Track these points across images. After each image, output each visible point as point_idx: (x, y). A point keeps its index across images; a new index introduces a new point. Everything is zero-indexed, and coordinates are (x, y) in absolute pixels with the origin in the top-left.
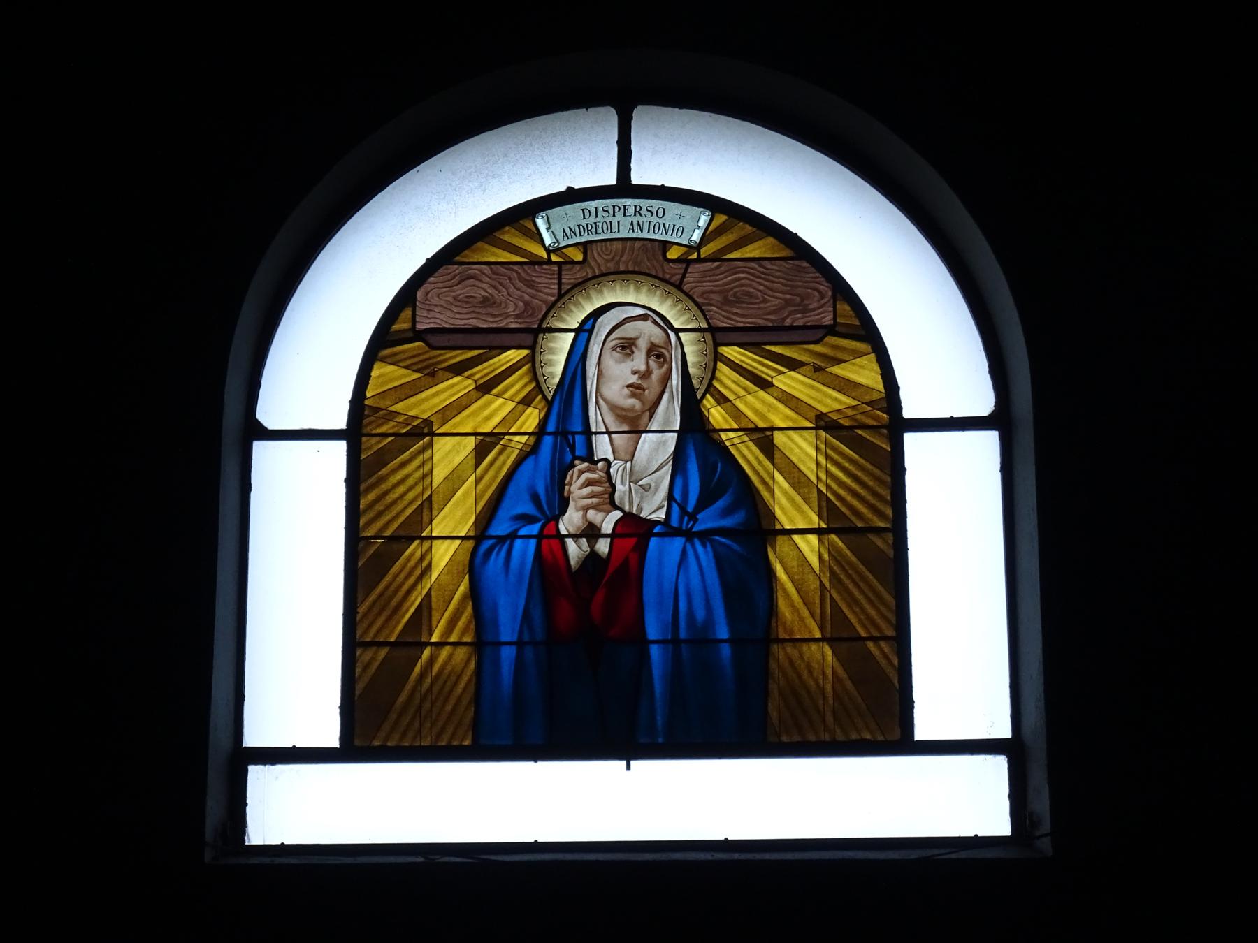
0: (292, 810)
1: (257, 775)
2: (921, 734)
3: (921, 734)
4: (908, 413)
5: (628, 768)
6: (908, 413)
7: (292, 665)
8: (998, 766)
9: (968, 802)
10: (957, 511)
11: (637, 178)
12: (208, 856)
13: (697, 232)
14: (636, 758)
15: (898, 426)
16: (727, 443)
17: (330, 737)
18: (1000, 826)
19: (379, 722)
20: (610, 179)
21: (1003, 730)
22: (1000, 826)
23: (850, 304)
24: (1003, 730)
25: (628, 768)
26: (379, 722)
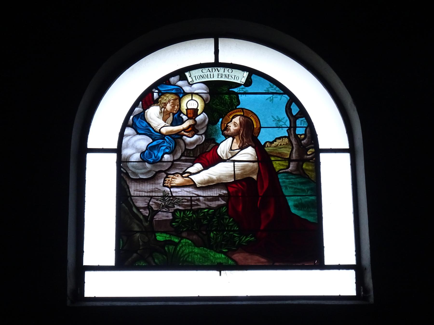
0: (98, 286)
1: (88, 275)
2: (327, 263)
3: (327, 263)
4: (321, 147)
5: (220, 275)
6: (321, 147)
7: (99, 237)
8: (352, 273)
9: (343, 285)
10: (337, 179)
11: (221, 60)
12: (69, 303)
13: (243, 78)
14: (223, 270)
15: (318, 151)
16: (281, 184)
17: (112, 263)
18: (353, 293)
19: (129, 257)
20: (212, 60)
21: (353, 262)
22: (353, 293)
23: (306, 119)
24: (353, 262)
25: (220, 275)
26: (129, 257)
